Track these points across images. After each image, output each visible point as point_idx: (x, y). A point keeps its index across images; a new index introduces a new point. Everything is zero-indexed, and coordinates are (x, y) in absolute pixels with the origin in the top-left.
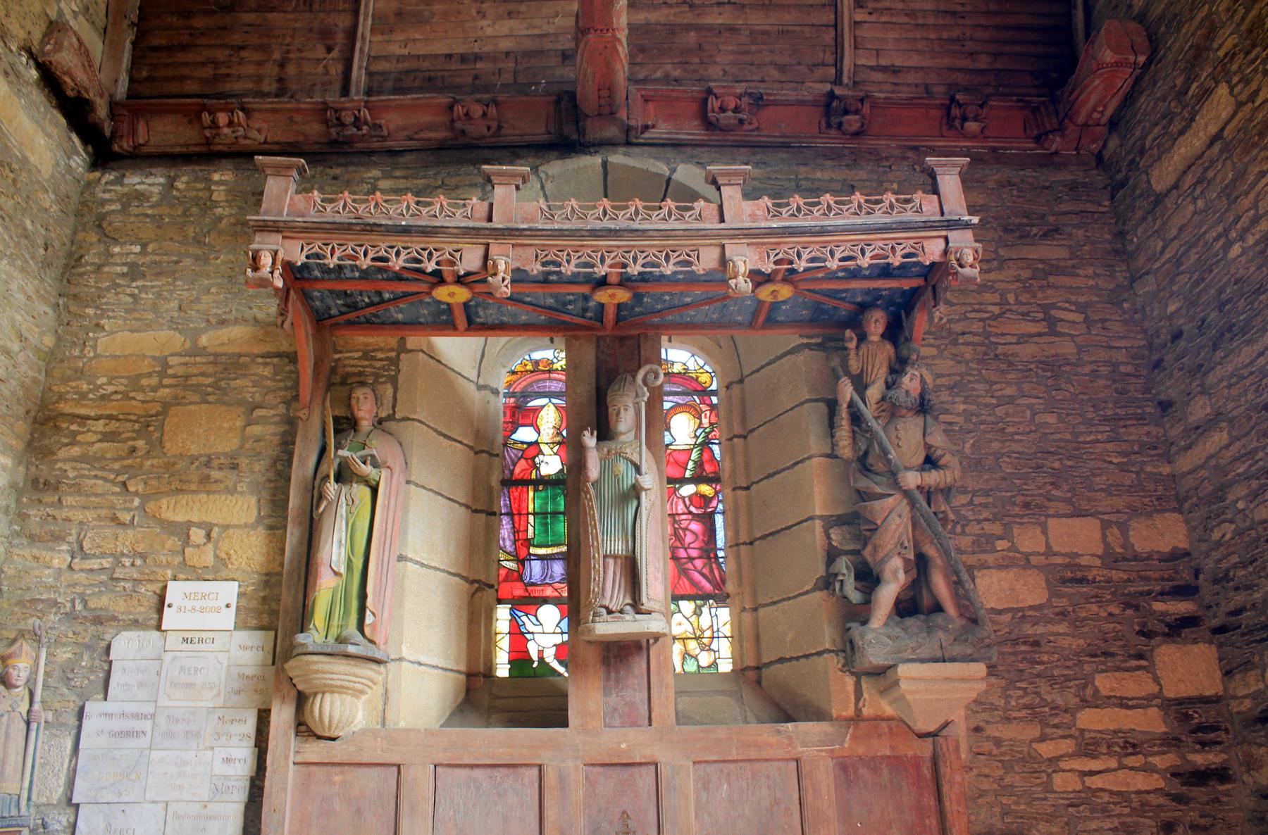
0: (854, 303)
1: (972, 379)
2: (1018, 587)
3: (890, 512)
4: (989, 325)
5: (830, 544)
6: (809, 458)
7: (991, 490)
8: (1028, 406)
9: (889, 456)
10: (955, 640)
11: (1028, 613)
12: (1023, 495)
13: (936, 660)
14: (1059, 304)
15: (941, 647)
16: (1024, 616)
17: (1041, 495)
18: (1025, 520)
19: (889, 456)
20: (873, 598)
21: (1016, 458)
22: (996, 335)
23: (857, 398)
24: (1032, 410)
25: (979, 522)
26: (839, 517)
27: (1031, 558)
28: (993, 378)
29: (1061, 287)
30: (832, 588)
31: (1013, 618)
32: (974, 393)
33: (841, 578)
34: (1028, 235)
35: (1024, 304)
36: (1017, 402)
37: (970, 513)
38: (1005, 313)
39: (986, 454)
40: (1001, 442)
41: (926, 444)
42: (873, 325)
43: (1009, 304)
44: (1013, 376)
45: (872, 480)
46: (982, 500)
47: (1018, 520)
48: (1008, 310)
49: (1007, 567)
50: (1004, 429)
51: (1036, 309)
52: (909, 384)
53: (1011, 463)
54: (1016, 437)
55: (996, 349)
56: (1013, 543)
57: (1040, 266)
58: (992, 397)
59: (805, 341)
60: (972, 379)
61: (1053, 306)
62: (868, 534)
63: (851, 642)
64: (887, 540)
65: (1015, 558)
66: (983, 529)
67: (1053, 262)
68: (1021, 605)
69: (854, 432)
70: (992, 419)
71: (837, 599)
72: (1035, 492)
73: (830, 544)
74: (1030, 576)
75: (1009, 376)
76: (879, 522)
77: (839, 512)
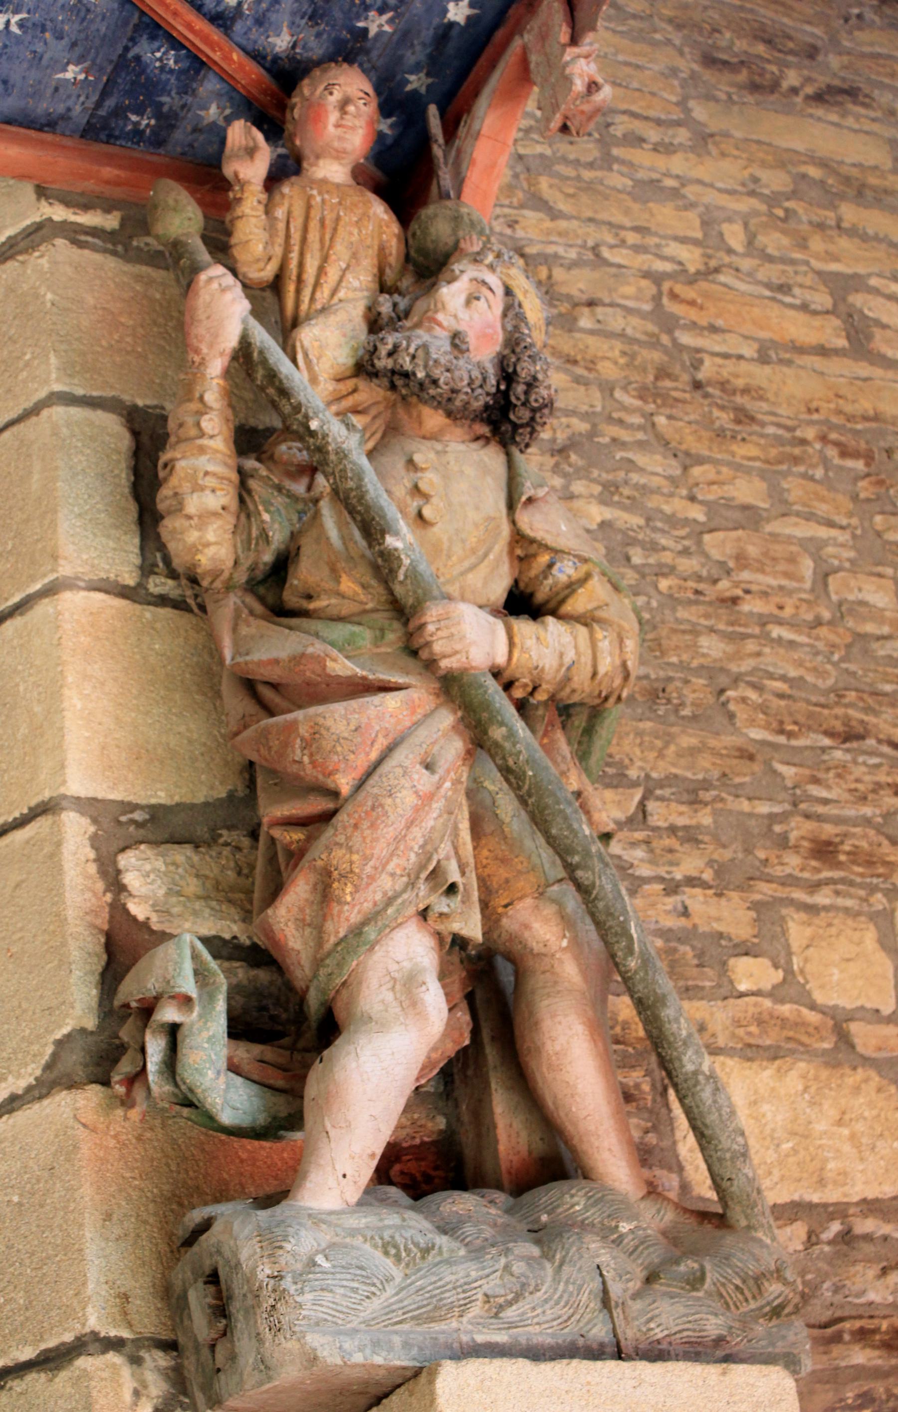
0: (257, 56)
1: (625, 435)
2: (821, 1127)
3: (389, 751)
4: (674, 296)
5: (118, 910)
6: (50, 591)
7: (706, 785)
8: (804, 543)
9: (391, 541)
10: (651, 1279)
11: (867, 1225)
12: (807, 816)
13: (594, 1353)
14: (873, 282)
15: (606, 1301)
16: (847, 1237)
17: (867, 821)
18: (823, 898)
19: (391, 541)
20: (311, 1089)
21: (781, 696)
22: (693, 326)
23: (262, 337)
24: (818, 559)
25: (672, 888)
26: (157, 813)
27: (854, 1028)
28: (692, 444)
29: (877, 238)
30: (126, 1067)
31: (812, 1239)
32: (635, 477)
33: (169, 1014)
34: (774, 87)
35: (770, 259)
36: (769, 528)
37: (639, 853)
38: (717, 270)
39: (682, 666)
40: (730, 637)
41: (519, 538)
42: (333, 117)
43: (730, 251)
44: (754, 452)
45: (317, 635)
46: (680, 815)
47: (799, 895)
48: (729, 266)
49: (774, 1054)
50: (735, 600)
51: (808, 280)
52: (464, 315)
53: (764, 708)
54: (776, 631)
55: (697, 365)
56: (789, 972)
57: (814, 172)
58: (692, 499)
59: (59, 213)
60: (625, 435)
61: (856, 283)
62: (296, 836)
63: (213, 1278)
64: (381, 849)
65: (800, 1024)
66: (685, 912)
67: (844, 170)
68: (832, 1195)
69: (243, 475)
70: (688, 565)
71: (154, 1109)
72: (850, 812)
73: (118, 910)
74: (857, 1090)
75: (741, 450)
76: (344, 783)
77: (161, 797)
